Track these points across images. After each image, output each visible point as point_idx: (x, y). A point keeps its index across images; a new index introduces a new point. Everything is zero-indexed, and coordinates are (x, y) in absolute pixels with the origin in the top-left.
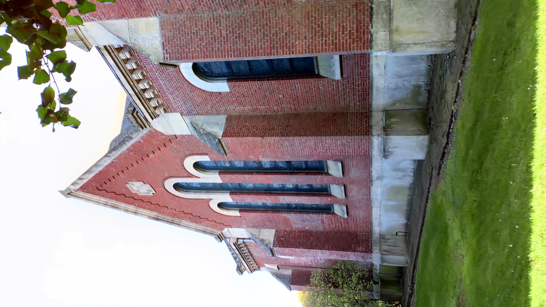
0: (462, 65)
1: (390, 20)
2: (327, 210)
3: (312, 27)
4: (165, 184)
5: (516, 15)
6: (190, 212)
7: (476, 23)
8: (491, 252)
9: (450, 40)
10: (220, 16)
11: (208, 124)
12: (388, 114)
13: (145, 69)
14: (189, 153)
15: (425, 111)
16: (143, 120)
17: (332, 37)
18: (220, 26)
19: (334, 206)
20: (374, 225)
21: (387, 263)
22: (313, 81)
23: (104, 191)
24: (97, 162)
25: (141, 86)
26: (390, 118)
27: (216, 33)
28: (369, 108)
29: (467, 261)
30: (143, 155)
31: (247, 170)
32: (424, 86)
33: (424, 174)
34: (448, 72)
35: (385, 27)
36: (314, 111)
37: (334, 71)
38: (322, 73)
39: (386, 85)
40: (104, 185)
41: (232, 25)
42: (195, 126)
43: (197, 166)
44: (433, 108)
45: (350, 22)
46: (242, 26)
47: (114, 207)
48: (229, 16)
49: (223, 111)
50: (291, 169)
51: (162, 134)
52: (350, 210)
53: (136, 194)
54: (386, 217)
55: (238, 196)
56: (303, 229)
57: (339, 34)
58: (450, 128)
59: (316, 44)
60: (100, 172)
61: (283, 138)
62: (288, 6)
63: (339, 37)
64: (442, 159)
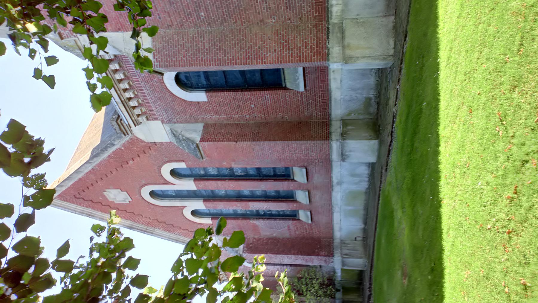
1: (343, 38)
2: (293, 216)
3: (281, 43)
4: (142, 191)
6: (164, 220)
7: (407, 39)
8: (420, 212)
9: (390, 54)
10: (203, 31)
11: (187, 130)
12: (345, 122)
14: (166, 159)
15: (375, 121)
16: (126, 127)
18: (204, 39)
21: (348, 266)
22: (280, 92)
25: (127, 95)
26: (347, 126)
27: (200, 45)
29: (406, 232)
31: (220, 177)
33: (376, 172)
34: (391, 82)
35: (339, 43)
37: (299, 84)
38: (288, 86)
39: (342, 97)
40: (82, 193)
41: (214, 39)
42: (175, 132)
43: (174, 173)
44: (381, 116)
45: (311, 39)
46: (222, 40)
47: (90, 215)
48: (211, 31)
49: (200, 119)
50: (260, 175)
51: (142, 141)
53: (113, 202)
54: (345, 223)
55: (211, 203)
56: (271, 236)
57: (303, 49)
59: (283, 56)
60: (80, 179)
61: (254, 143)
64: (388, 156)
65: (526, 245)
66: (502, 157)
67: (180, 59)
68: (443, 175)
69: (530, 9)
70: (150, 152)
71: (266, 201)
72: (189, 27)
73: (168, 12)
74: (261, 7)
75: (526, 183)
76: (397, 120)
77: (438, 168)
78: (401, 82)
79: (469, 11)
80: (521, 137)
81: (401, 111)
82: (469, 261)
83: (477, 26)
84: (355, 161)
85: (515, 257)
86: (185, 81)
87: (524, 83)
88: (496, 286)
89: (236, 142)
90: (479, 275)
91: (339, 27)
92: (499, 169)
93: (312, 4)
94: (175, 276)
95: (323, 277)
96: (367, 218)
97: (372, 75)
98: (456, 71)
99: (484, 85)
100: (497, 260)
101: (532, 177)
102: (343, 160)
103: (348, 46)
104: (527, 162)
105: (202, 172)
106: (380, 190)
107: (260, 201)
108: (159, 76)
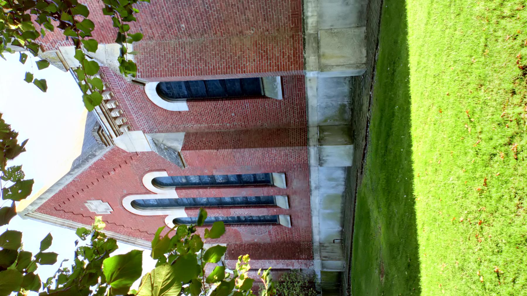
0: (371, 80)
1: (318, 47)
2: (273, 221)
3: (259, 53)
4: (123, 201)
5: (398, 36)
9: (363, 62)
10: (184, 42)
11: (168, 140)
12: (321, 129)
13: (113, 90)
14: (148, 169)
15: (349, 127)
16: (107, 138)
17: (275, 60)
18: (185, 50)
19: (280, 217)
20: (314, 234)
21: (327, 268)
22: (259, 101)
23: (62, 212)
24: (59, 180)
25: (109, 106)
26: (323, 132)
27: (181, 56)
28: (306, 124)
29: (383, 230)
30: (104, 172)
31: (201, 185)
32: (348, 105)
33: (352, 175)
35: (315, 53)
36: (261, 128)
37: (277, 92)
38: (267, 94)
39: (318, 104)
40: (63, 205)
41: (195, 49)
42: (156, 142)
43: (156, 182)
44: (355, 122)
45: (288, 49)
46: (203, 51)
48: (192, 43)
49: (182, 128)
50: (241, 182)
51: (124, 152)
52: (293, 220)
54: (324, 227)
55: (192, 211)
56: (252, 242)
58: (367, 132)
59: (262, 66)
60: (60, 191)
61: (235, 150)
62: (240, 36)
63: (281, 60)
64: (363, 160)
65: (498, 234)
66: (472, 152)
67: (162, 69)
68: (415, 173)
69: (492, 13)
70: (132, 162)
71: (247, 207)
72: (170, 38)
73: (150, 25)
74: (240, 19)
75: (495, 175)
76: (371, 125)
77: (411, 166)
78: (374, 88)
79: (436, 17)
80: (488, 132)
81: (375, 115)
82: (444, 254)
83: (443, 31)
84: (332, 165)
85: (487, 246)
86: (166, 90)
87: (489, 81)
88: (471, 276)
89: (218, 149)
90: (454, 267)
91: (315, 38)
92: (469, 164)
93: (289, 16)
94: (167, 264)
95: (304, 279)
96: (344, 221)
97: (345, 83)
98: (426, 74)
99: (453, 86)
100: (471, 251)
101: (499, 169)
102: (321, 164)
103: (323, 55)
104: (495, 155)
105: (184, 181)
106: (356, 193)
107: (241, 207)
108: (141, 87)
